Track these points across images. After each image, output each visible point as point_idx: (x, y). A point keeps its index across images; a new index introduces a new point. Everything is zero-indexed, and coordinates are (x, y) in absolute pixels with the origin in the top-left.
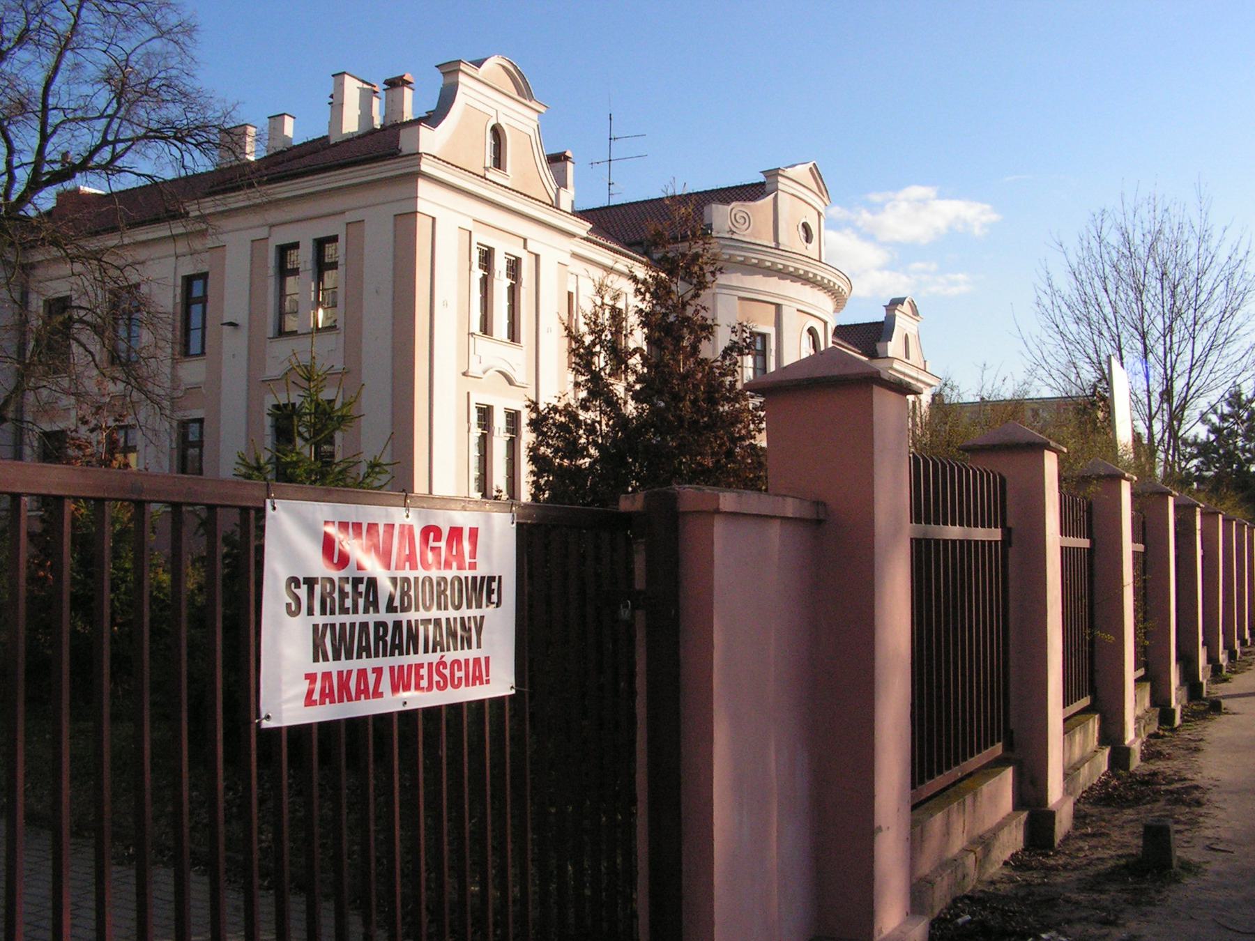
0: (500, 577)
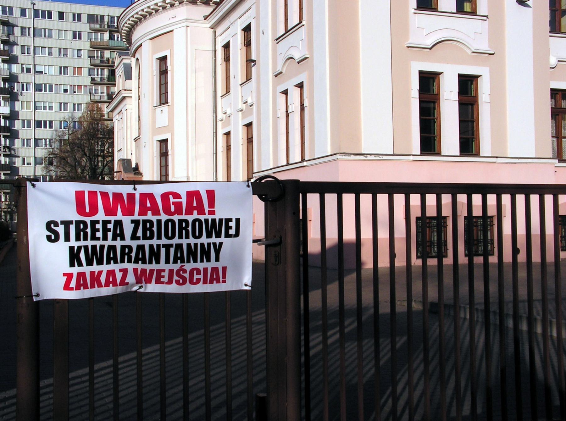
0: (238, 221)
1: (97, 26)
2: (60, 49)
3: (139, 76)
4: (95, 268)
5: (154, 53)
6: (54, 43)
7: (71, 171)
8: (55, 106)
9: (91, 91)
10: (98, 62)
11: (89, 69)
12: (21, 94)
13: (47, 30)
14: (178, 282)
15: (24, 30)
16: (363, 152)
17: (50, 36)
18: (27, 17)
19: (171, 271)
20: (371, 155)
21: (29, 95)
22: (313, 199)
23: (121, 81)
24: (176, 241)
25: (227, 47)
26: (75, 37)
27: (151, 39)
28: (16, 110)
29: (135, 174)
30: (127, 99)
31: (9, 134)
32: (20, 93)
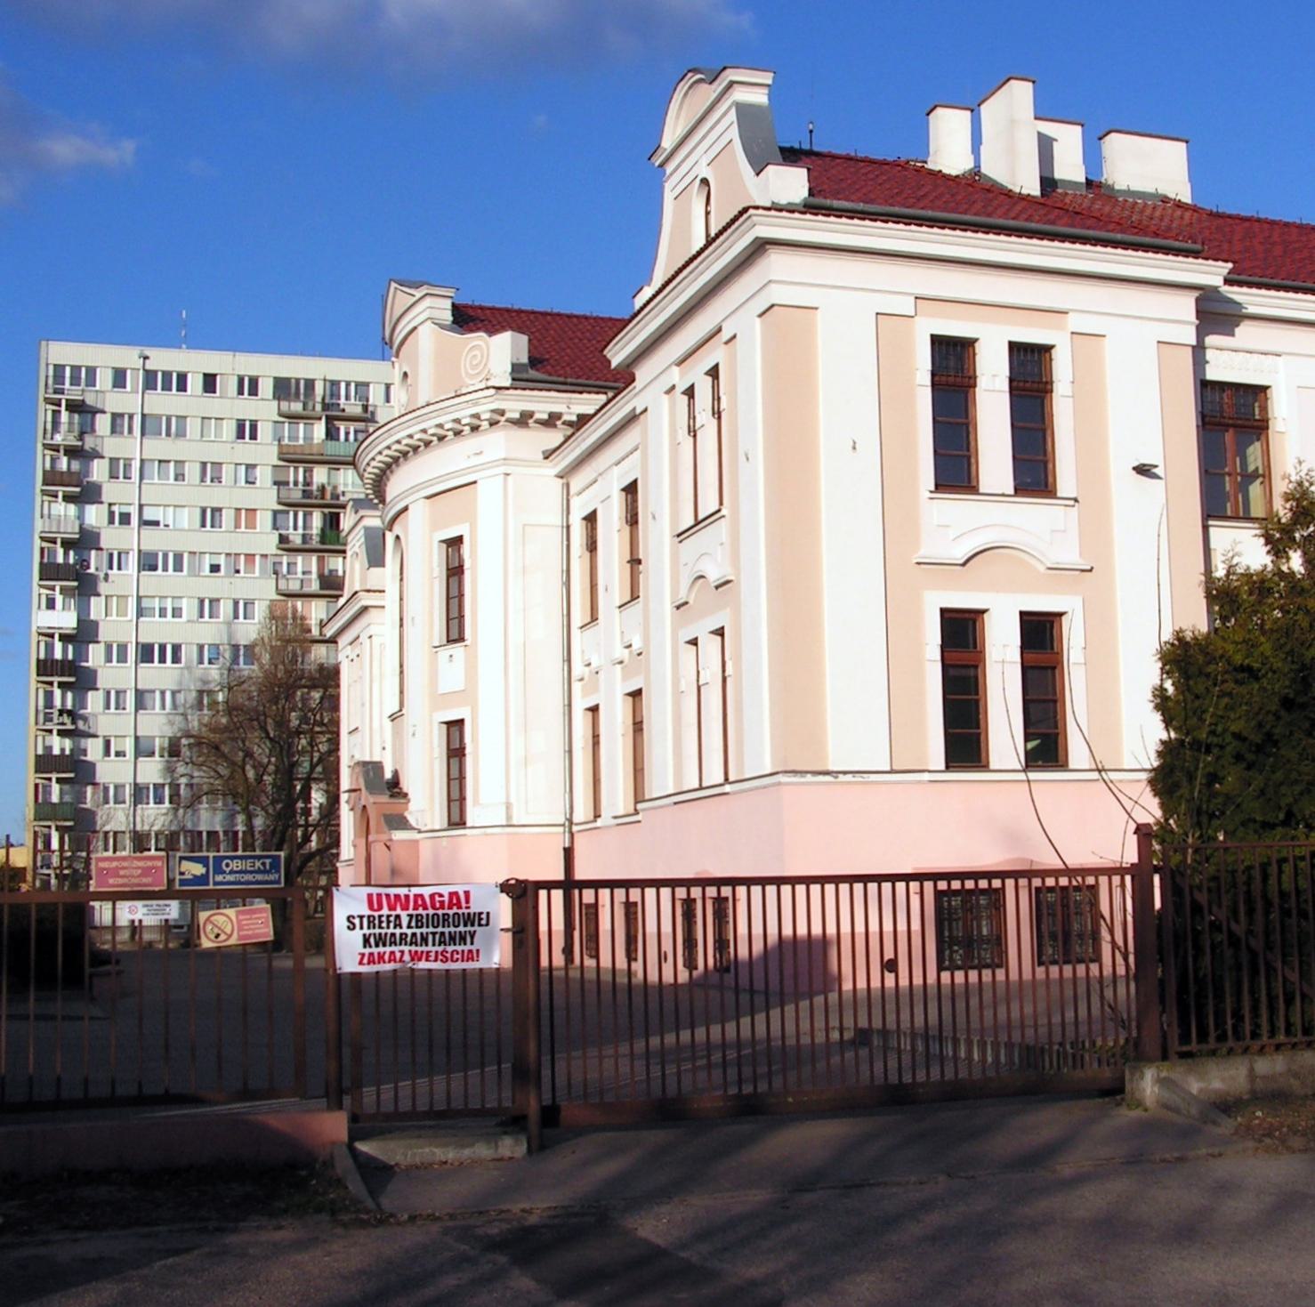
0: (488, 914)
1: (297, 407)
2: (204, 464)
3: (401, 573)
4: (381, 949)
5: (435, 526)
6: (190, 450)
7: (231, 777)
8: (189, 608)
9: (278, 568)
10: (296, 495)
11: (275, 513)
12: (106, 577)
13: (174, 420)
14: (442, 960)
15: (119, 421)
16: (831, 768)
17: (181, 433)
18: (129, 388)
19: (437, 952)
20: (845, 773)
21: (124, 581)
22: (543, 894)
23: (357, 566)
24: (440, 929)
25: (591, 519)
26: (240, 435)
27: (428, 498)
28: (92, 617)
29: (391, 796)
30: (373, 613)
31: (72, 679)
32: (102, 575)
